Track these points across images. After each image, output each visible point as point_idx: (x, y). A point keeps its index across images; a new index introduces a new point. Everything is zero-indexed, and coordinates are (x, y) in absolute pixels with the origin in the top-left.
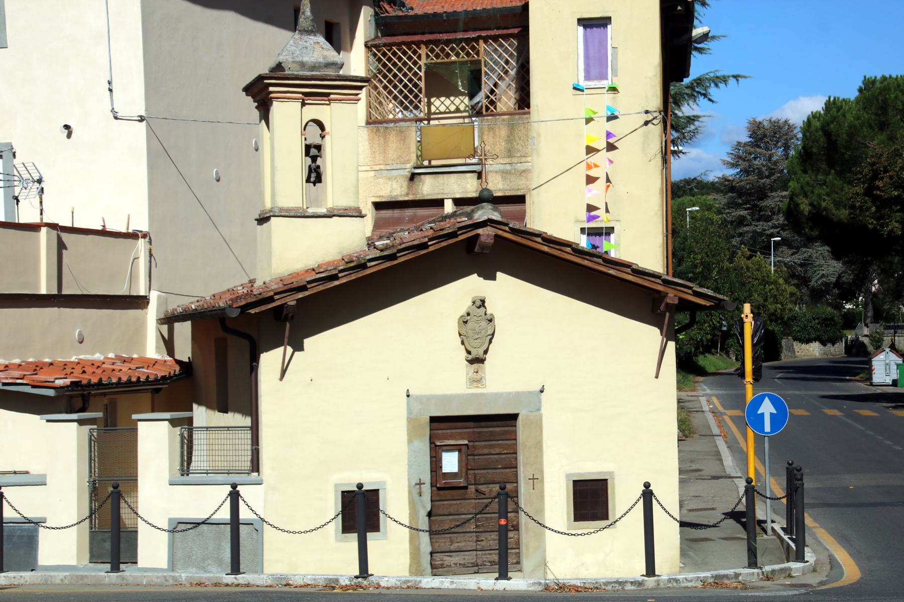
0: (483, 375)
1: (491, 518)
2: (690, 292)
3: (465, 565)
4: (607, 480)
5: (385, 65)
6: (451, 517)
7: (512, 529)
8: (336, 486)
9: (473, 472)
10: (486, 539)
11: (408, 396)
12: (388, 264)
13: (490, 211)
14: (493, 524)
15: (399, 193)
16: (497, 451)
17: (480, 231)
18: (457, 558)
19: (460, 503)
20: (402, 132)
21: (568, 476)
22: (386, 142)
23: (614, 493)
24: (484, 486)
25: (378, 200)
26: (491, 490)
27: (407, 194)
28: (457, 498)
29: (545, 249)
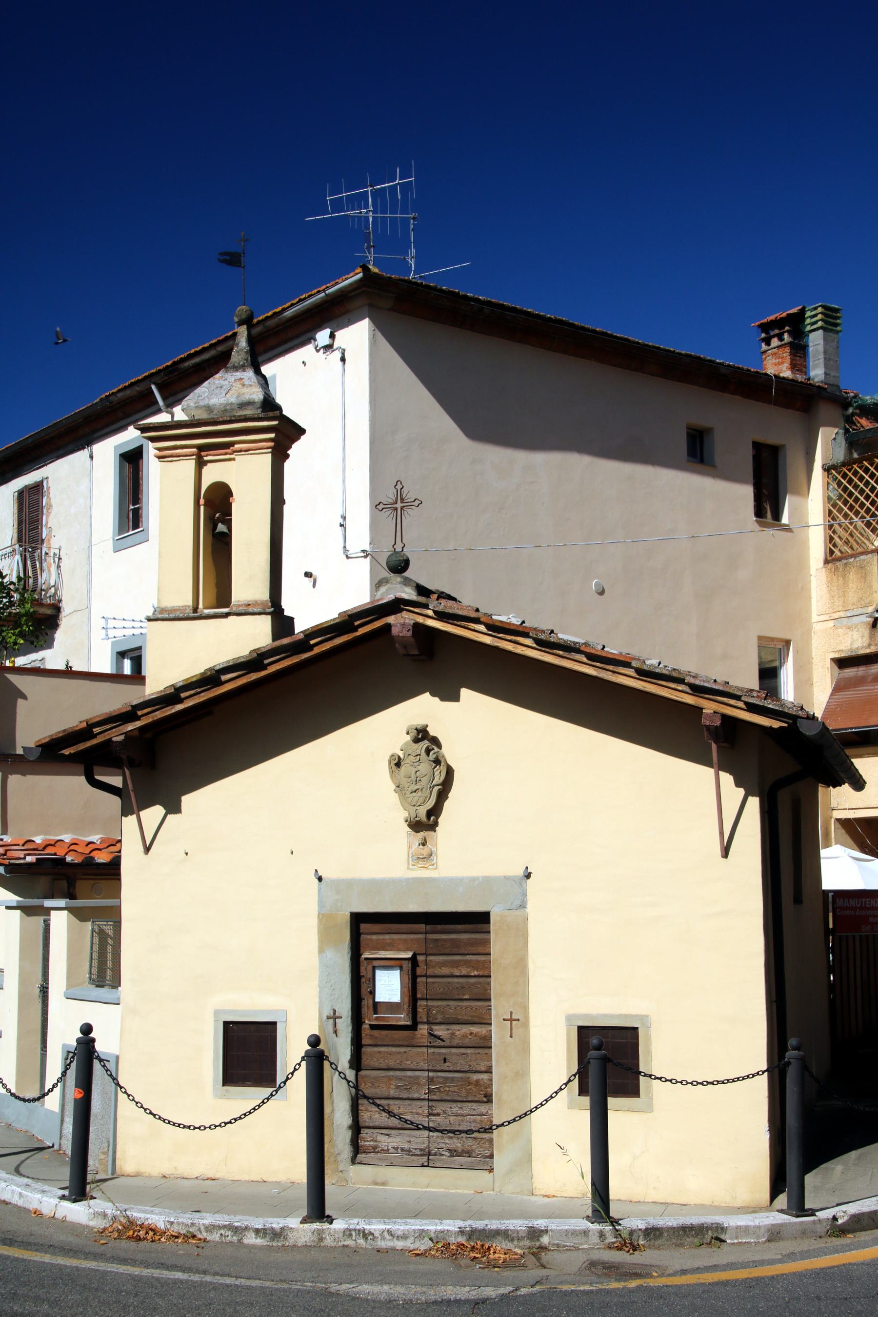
0: (434, 849)
1: (452, 1079)
2: (741, 704)
3: (409, 1151)
4: (637, 1028)
5: (845, 489)
6: (391, 1073)
7: (485, 1100)
8: (217, 1013)
9: (425, 1003)
10: (444, 1112)
11: (320, 879)
12: (254, 676)
13: (399, 586)
14: (456, 1089)
15: (860, 645)
16: (464, 972)
17: (391, 619)
18: (398, 1139)
19: (405, 1052)
20: (862, 567)
21: (569, 1018)
22: (845, 582)
23: (649, 1052)
24: (443, 1027)
25: (837, 656)
26: (453, 1034)
27: (870, 645)
28: (401, 1043)
29: (487, 640)
